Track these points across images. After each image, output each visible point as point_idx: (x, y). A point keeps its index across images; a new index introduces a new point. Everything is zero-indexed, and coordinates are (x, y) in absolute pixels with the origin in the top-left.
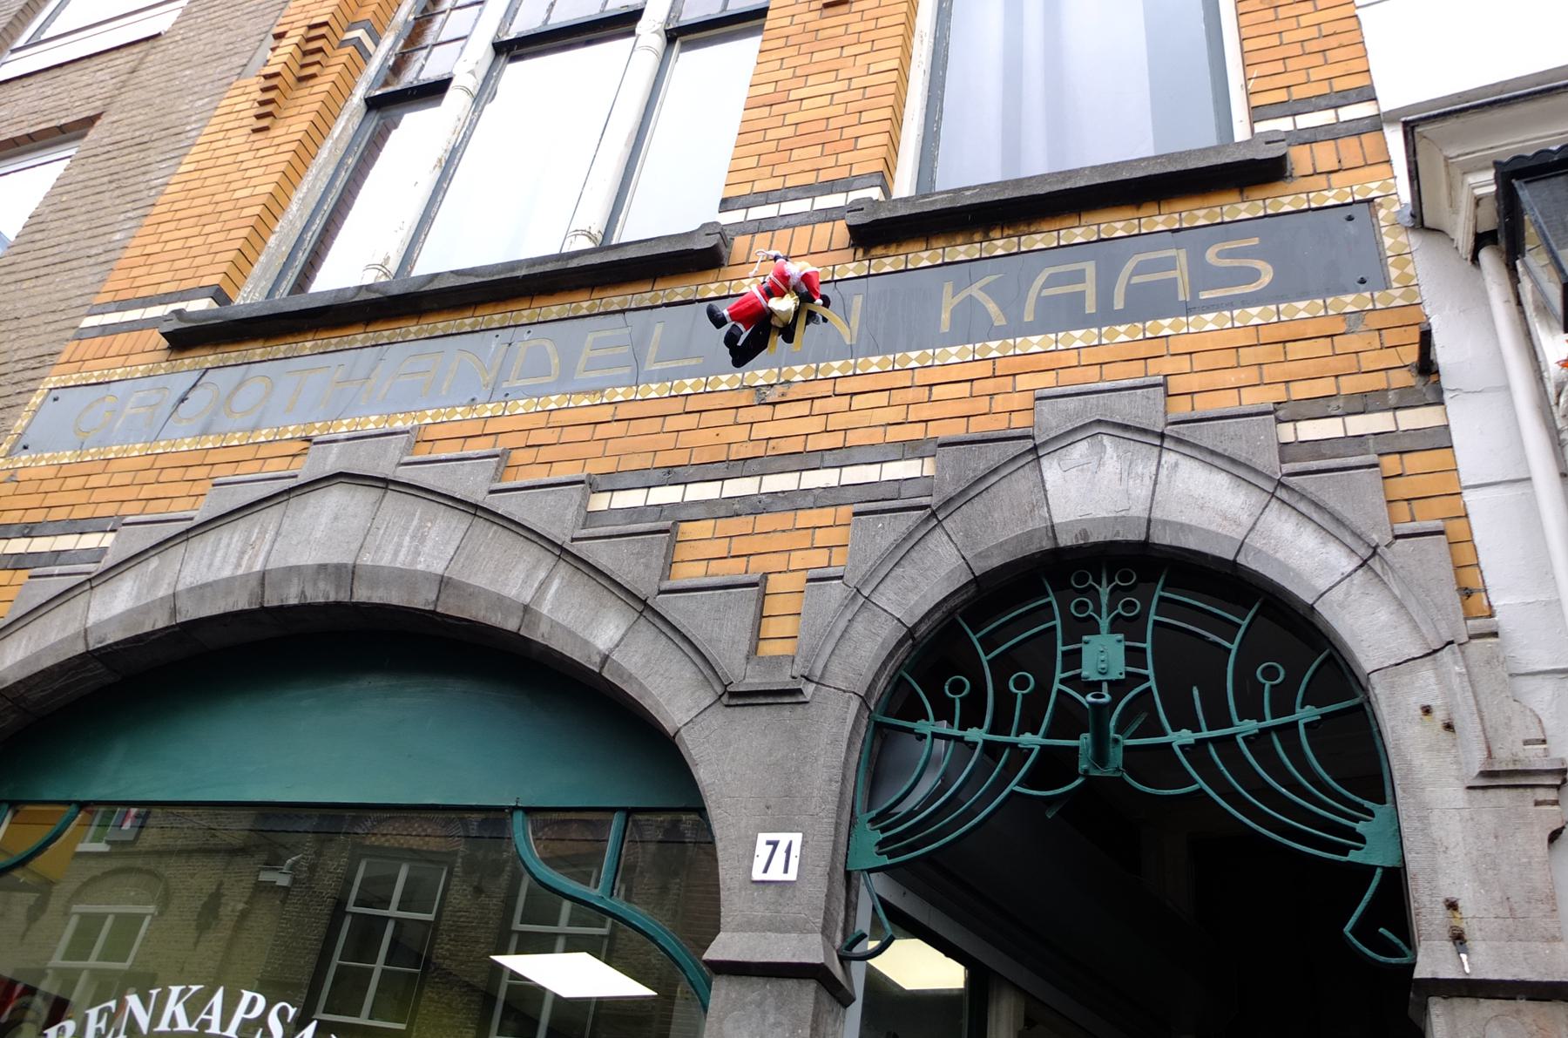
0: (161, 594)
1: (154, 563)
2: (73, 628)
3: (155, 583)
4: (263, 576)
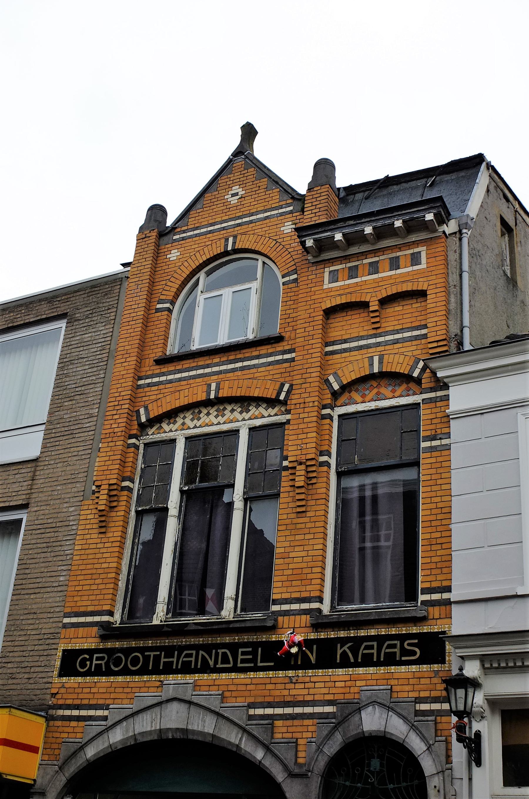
0: (130, 734)
1: (125, 723)
2: (106, 745)
3: (127, 731)
4: (160, 730)
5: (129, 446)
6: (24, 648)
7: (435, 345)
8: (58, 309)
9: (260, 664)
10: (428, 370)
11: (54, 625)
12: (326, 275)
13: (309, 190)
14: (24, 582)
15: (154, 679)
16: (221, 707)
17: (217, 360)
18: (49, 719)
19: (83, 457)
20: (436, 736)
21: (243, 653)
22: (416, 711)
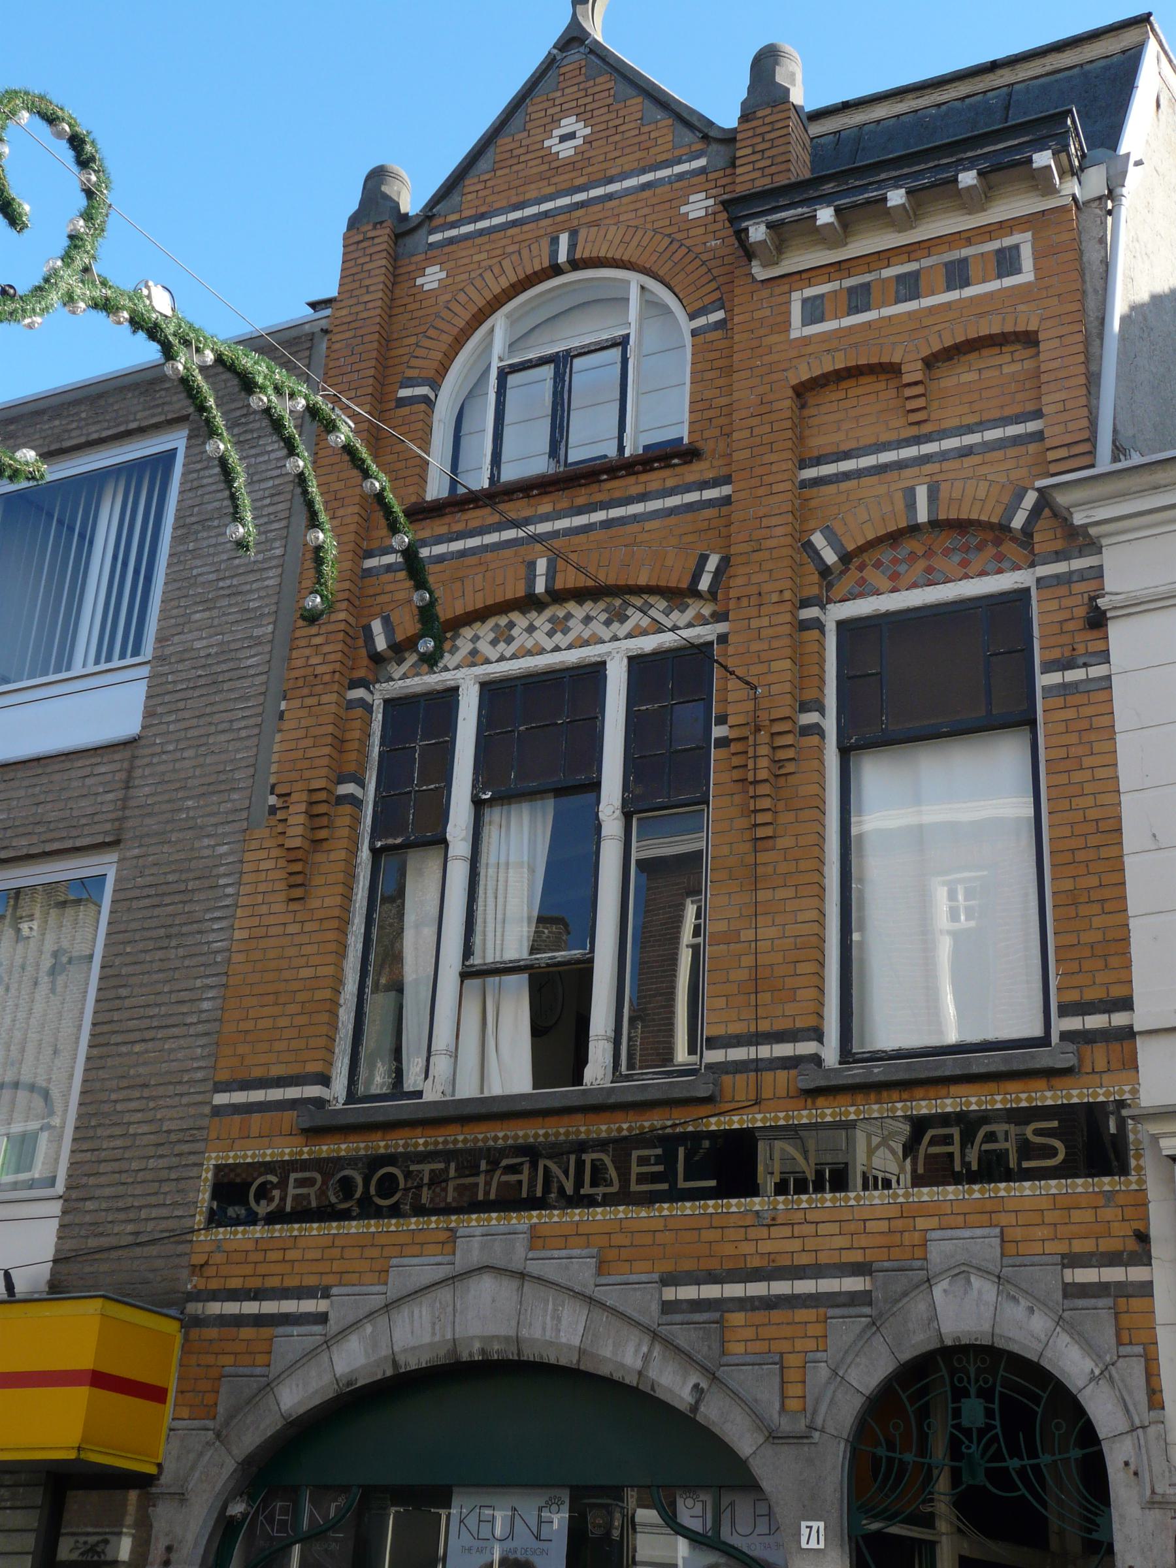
2: (327, 1378)
5: (351, 705)
6: (124, 1165)
7: (1063, 453)
8: (166, 408)
9: (682, 1184)
10: (1047, 512)
11: (192, 1111)
12: (796, 309)
13: (745, 118)
14: (116, 1016)
15: (433, 1226)
16: (597, 1286)
17: (545, 508)
18: (191, 1323)
19: (243, 733)
20: (1120, 1343)
21: (643, 1161)
22: (1066, 1285)
